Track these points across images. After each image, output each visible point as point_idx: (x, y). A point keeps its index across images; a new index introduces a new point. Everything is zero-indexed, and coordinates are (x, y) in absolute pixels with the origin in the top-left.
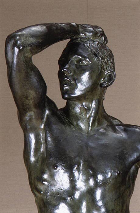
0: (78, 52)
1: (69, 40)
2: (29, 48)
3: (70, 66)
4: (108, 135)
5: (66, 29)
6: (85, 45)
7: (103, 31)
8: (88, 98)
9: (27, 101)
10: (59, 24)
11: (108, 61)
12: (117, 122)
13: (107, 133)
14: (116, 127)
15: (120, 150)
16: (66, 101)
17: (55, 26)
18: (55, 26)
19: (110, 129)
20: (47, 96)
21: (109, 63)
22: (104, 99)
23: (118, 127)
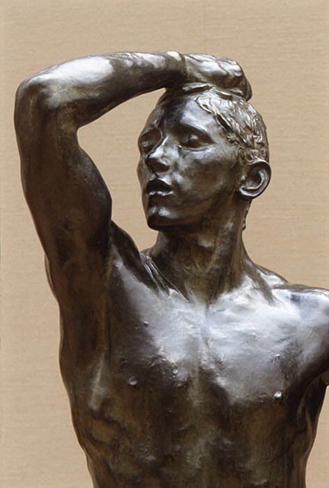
0: (183, 118)
1: (163, 90)
2: (70, 110)
3: (165, 151)
4: (254, 310)
5: (156, 66)
6: (200, 101)
7: (241, 71)
8: (207, 226)
9: (67, 233)
10: (140, 55)
11: (252, 140)
12: (275, 280)
13: (252, 306)
14: (274, 292)
15: (285, 344)
16: (157, 232)
17: (130, 59)
18: (130, 59)
19: (259, 296)
20: (113, 224)
21: (256, 145)
22: (244, 228)
23: (277, 292)
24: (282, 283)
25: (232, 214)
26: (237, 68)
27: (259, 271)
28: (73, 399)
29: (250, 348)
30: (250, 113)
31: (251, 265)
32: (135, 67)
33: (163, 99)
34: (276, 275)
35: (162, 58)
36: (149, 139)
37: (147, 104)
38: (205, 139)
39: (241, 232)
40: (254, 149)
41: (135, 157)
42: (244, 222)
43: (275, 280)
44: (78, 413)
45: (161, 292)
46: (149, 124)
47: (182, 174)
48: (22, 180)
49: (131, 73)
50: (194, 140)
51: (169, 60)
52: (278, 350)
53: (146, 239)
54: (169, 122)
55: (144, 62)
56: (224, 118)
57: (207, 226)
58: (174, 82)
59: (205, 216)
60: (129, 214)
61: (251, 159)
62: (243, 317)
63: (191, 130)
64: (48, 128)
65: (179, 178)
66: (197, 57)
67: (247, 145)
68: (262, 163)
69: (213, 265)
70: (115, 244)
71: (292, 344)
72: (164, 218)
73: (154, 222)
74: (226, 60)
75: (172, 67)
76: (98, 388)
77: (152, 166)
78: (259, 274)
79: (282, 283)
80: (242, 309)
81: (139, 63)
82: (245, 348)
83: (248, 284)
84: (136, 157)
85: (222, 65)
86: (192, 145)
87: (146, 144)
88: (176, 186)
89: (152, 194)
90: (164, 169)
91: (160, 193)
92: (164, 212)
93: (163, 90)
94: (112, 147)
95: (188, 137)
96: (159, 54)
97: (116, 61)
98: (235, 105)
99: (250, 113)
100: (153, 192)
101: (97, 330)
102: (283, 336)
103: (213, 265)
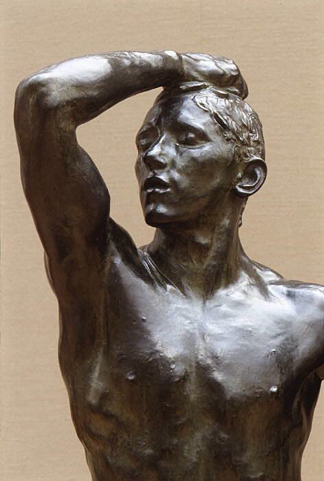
0: (181, 116)
1: (161, 89)
2: (69, 109)
3: (162, 149)
4: (250, 306)
5: (154, 65)
6: (197, 100)
7: (238, 70)
8: (203, 223)
9: (66, 229)
10: (138, 54)
11: (249, 138)
12: (271, 276)
13: (248, 302)
14: (270, 288)
15: (281, 339)
16: (155, 229)
17: (128, 59)
18: (128, 59)
19: (255, 292)
20: (111, 221)
21: (252, 142)
22: (241, 225)
23: (273, 288)
24: (278, 279)
25: (229, 211)
26: (233, 67)
27: (255, 267)
28: (72, 393)
29: (246, 343)
30: (246, 111)
31: (247, 261)
32: (133, 66)
33: (161, 97)
34: (272, 271)
35: (160, 57)
36: (147, 137)
37: (144, 102)
38: (202, 137)
39: (238, 229)
40: (250, 146)
41: (133, 155)
42: (241, 219)
43: (271, 276)
44: (77, 408)
45: (159, 288)
46: (147, 122)
47: (179, 171)
48: (22, 178)
49: (129, 72)
50: (191, 138)
51: (167, 59)
52: (274, 345)
53: (143, 236)
54: (166, 120)
55: (142, 61)
56: (220, 117)
57: (203, 223)
58: (171, 81)
59: (202, 213)
60: (127, 211)
61: (247, 157)
62: (239, 312)
63: (188, 128)
64: (47, 126)
65: (176, 176)
66: (194, 56)
67: (243, 143)
68: (258, 160)
69: (209, 261)
70: (113, 240)
71: (287, 339)
72: (161, 215)
73: (151, 218)
74: (222, 59)
75: (170, 66)
76: (97, 383)
77: (150, 163)
78: (255, 270)
79: (278, 279)
80: (238, 304)
81: (137, 62)
82: (241, 343)
83: (244, 280)
84: (134, 154)
85: (219, 64)
86: (189, 143)
87: (144, 142)
88: (173, 183)
89: (149, 191)
90: (162, 166)
91: (157, 190)
92: (162, 209)
93: (161, 89)
94: (110, 145)
95: (186, 135)
96: (157, 54)
97: (114, 60)
98: (231, 103)
99: (246, 111)
100: (151, 189)
101: (95, 326)
102: (279, 331)
103: (209, 261)
